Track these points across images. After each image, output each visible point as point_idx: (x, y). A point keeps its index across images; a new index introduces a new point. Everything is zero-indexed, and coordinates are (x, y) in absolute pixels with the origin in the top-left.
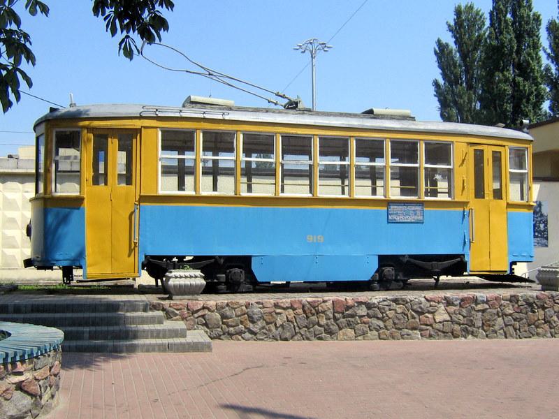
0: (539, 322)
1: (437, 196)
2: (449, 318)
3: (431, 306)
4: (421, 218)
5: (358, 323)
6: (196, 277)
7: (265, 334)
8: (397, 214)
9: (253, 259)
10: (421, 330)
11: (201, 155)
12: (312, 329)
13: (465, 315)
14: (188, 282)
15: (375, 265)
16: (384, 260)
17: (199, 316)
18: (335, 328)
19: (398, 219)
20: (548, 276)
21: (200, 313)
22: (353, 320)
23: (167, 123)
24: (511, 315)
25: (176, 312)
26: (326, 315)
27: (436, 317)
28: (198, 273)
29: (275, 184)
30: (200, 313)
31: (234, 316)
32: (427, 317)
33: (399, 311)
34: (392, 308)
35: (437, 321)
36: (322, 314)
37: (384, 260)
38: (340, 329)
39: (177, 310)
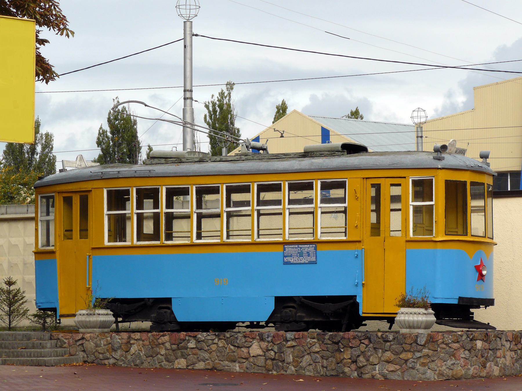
0: (345, 361)
1: (201, 239)
2: (261, 353)
3: (246, 341)
4: (313, 259)
5: (190, 355)
6: (107, 314)
7: (123, 360)
8: (291, 256)
9: (172, 300)
10: (239, 362)
11: (319, 205)
12: (156, 358)
13: (276, 351)
14: (416, 318)
15: (271, 307)
16: (281, 302)
17: (80, 345)
18: (173, 357)
19: (292, 261)
20: (407, 318)
21: (80, 342)
22: (185, 351)
23: (64, 176)
24: (317, 352)
25: (65, 341)
26: (165, 347)
27: (251, 352)
28: (109, 312)
29: (313, 233)
30: (80, 342)
31: (102, 345)
32: (243, 351)
33: (221, 345)
34: (215, 342)
35: (252, 355)
36: (162, 346)
37: (281, 302)
38: (177, 359)
39: (66, 339)
